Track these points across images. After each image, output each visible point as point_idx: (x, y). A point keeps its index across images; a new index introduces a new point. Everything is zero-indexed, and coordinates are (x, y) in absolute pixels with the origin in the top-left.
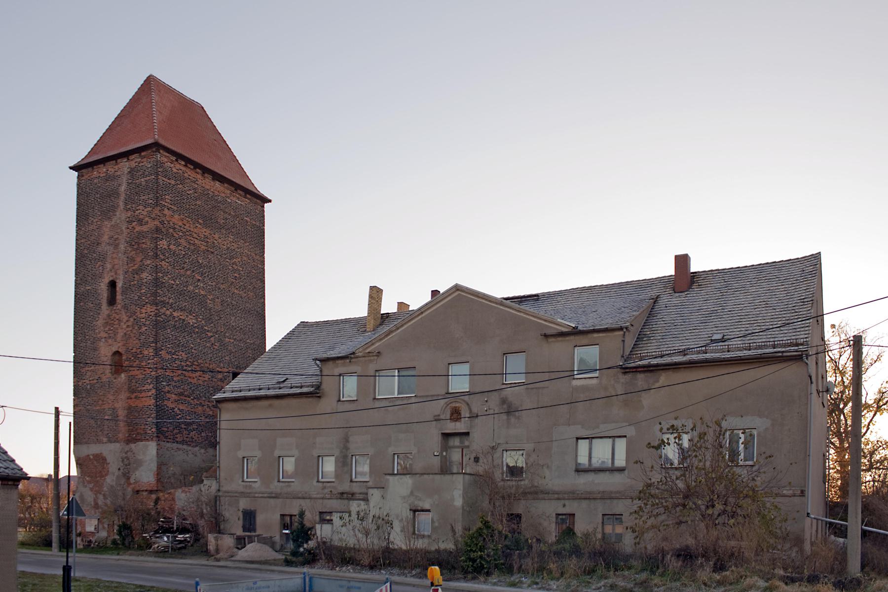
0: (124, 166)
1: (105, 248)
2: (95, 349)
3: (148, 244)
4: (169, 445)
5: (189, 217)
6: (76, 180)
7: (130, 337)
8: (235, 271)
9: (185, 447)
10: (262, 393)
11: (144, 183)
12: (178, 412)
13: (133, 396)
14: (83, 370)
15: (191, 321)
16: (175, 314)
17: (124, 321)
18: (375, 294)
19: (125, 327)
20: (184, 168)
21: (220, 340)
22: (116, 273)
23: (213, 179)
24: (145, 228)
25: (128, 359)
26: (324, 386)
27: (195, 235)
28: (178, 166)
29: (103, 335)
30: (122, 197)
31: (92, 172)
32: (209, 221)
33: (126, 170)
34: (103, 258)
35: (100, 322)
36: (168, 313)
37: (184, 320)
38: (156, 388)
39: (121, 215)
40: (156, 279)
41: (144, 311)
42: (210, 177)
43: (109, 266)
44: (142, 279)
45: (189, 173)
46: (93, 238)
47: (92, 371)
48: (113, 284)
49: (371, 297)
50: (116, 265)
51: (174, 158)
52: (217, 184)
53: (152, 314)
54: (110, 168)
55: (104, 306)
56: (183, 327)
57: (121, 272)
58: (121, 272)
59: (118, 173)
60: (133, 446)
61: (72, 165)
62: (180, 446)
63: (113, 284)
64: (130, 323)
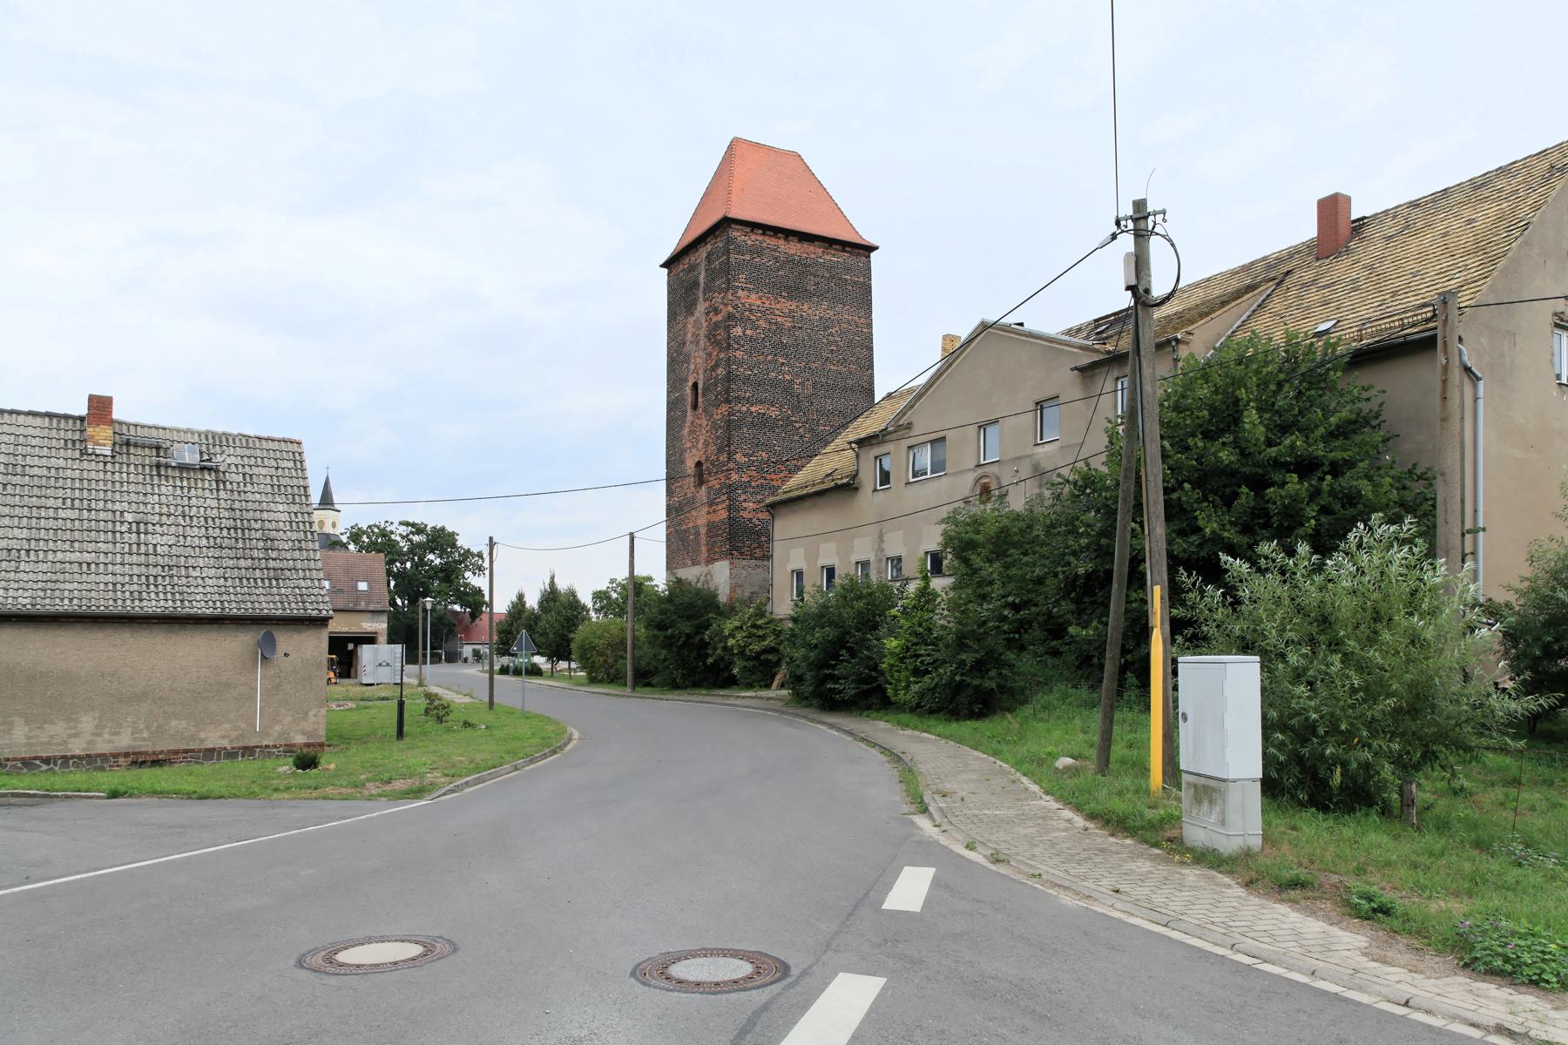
0: (703, 252)
1: (690, 347)
2: (682, 462)
8: (830, 343)
15: (774, 413)
23: (800, 241)
24: (719, 318)
28: (753, 237)
29: (688, 445)
32: (795, 291)
34: (687, 359)
35: (686, 431)
39: (701, 307)
45: (770, 241)
48: (695, 385)
52: (805, 245)
54: (692, 258)
56: (763, 422)
63: (695, 385)
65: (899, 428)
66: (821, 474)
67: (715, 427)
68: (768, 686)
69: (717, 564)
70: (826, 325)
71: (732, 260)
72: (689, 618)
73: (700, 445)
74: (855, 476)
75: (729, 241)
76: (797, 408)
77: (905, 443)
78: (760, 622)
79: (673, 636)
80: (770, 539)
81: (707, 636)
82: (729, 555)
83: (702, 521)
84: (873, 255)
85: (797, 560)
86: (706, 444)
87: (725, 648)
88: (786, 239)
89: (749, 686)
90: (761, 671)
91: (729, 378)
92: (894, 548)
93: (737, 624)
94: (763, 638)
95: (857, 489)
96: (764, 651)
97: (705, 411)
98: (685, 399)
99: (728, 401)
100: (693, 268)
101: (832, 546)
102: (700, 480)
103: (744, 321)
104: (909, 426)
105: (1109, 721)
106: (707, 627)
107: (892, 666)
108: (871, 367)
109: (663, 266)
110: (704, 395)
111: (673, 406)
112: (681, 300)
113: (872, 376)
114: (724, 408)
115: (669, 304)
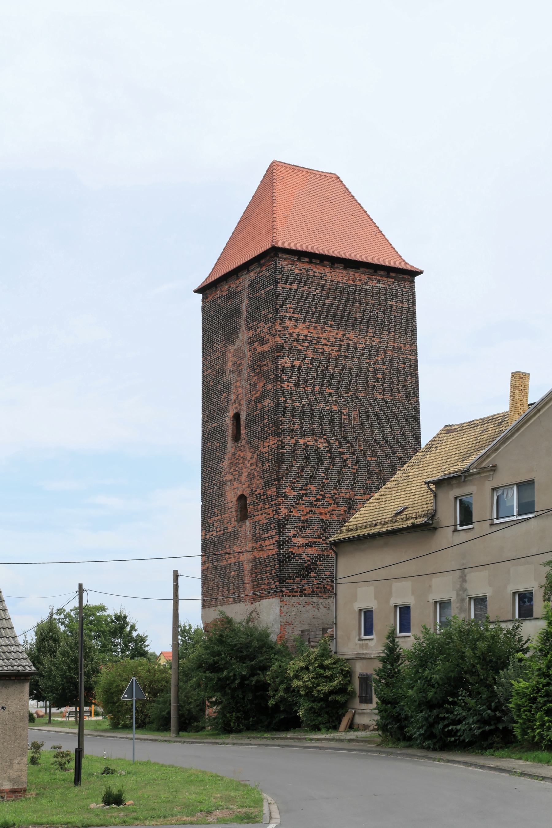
0: (246, 280)
1: (229, 377)
2: (222, 495)
3: (269, 365)
4: (295, 600)
5: (316, 322)
6: (200, 304)
7: (254, 477)
8: (376, 371)
9: (315, 600)
10: (376, 530)
11: (263, 296)
12: (307, 558)
13: (257, 546)
14: (210, 521)
15: (321, 444)
16: (302, 441)
17: (248, 458)
18: (519, 381)
19: (249, 465)
20: (307, 266)
21: (358, 461)
22: (240, 405)
23: (345, 268)
24: (266, 348)
25: (253, 503)
26: (439, 515)
27: (324, 342)
28: (300, 266)
29: (229, 477)
30: (244, 316)
31: (216, 291)
32: (342, 320)
33: (247, 283)
34: (227, 388)
35: (226, 463)
36: (293, 441)
37: (312, 446)
38: (279, 534)
39: (244, 336)
40: (278, 405)
41: (266, 444)
42: (341, 266)
43: (233, 397)
44: (264, 407)
45: (317, 270)
46: (218, 367)
47: (219, 520)
48: (237, 417)
49: (513, 386)
50: (240, 395)
51: (295, 258)
53: (275, 446)
54: (233, 285)
55: (230, 444)
56: (312, 454)
57: (244, 402)
58: (244, 402)
59: (240, 288)
60: (257, 604)
61: (196, 287)
62: (309, 599)
63: (237, 417)
64: (254, 460)
65: (483, 470)
66: (388, 515)
67: (261, 459)
68: (335, 728)
69: (265, 602)
70: (371, 352)
71: (280, 290)
72: (242, 659)
73: (243, 478)
74: (433, 515)
75: (277, 270)
76: (344, 440)
77: (489, 485)
78: (327, 662)
79: (227, 678)
80: (333, 578)
81: (268, 677)
82: (278, 592)
83: (246, 557)
84: (417, 279)
85: (366, 598)
86: (251, 477)
87: (288, 690)
88: (332, 267)
89: (316, 728)
90: (329, 711)
91: (278, 409)
92: (478, 585)
93: (302, 664)
94: (330, 679)
95: (435, 529)
96: (331, 693)
97: (249, 442)
98: (225, 429)
99: (277, 434)
100: (232, 295)
101: (407, 584)
102: (243, 513)
103: (292, 351)
104: (494, 469)
105: (80, 724)
106: (264, 668)
107: (519, 707)
108: (416, 394)
109: (197, 291)
110: (247, 426)
111: (210, 437)
112: (218, 326)
113: (417, 404)
114: (272, 441)
115: (204, 330)
